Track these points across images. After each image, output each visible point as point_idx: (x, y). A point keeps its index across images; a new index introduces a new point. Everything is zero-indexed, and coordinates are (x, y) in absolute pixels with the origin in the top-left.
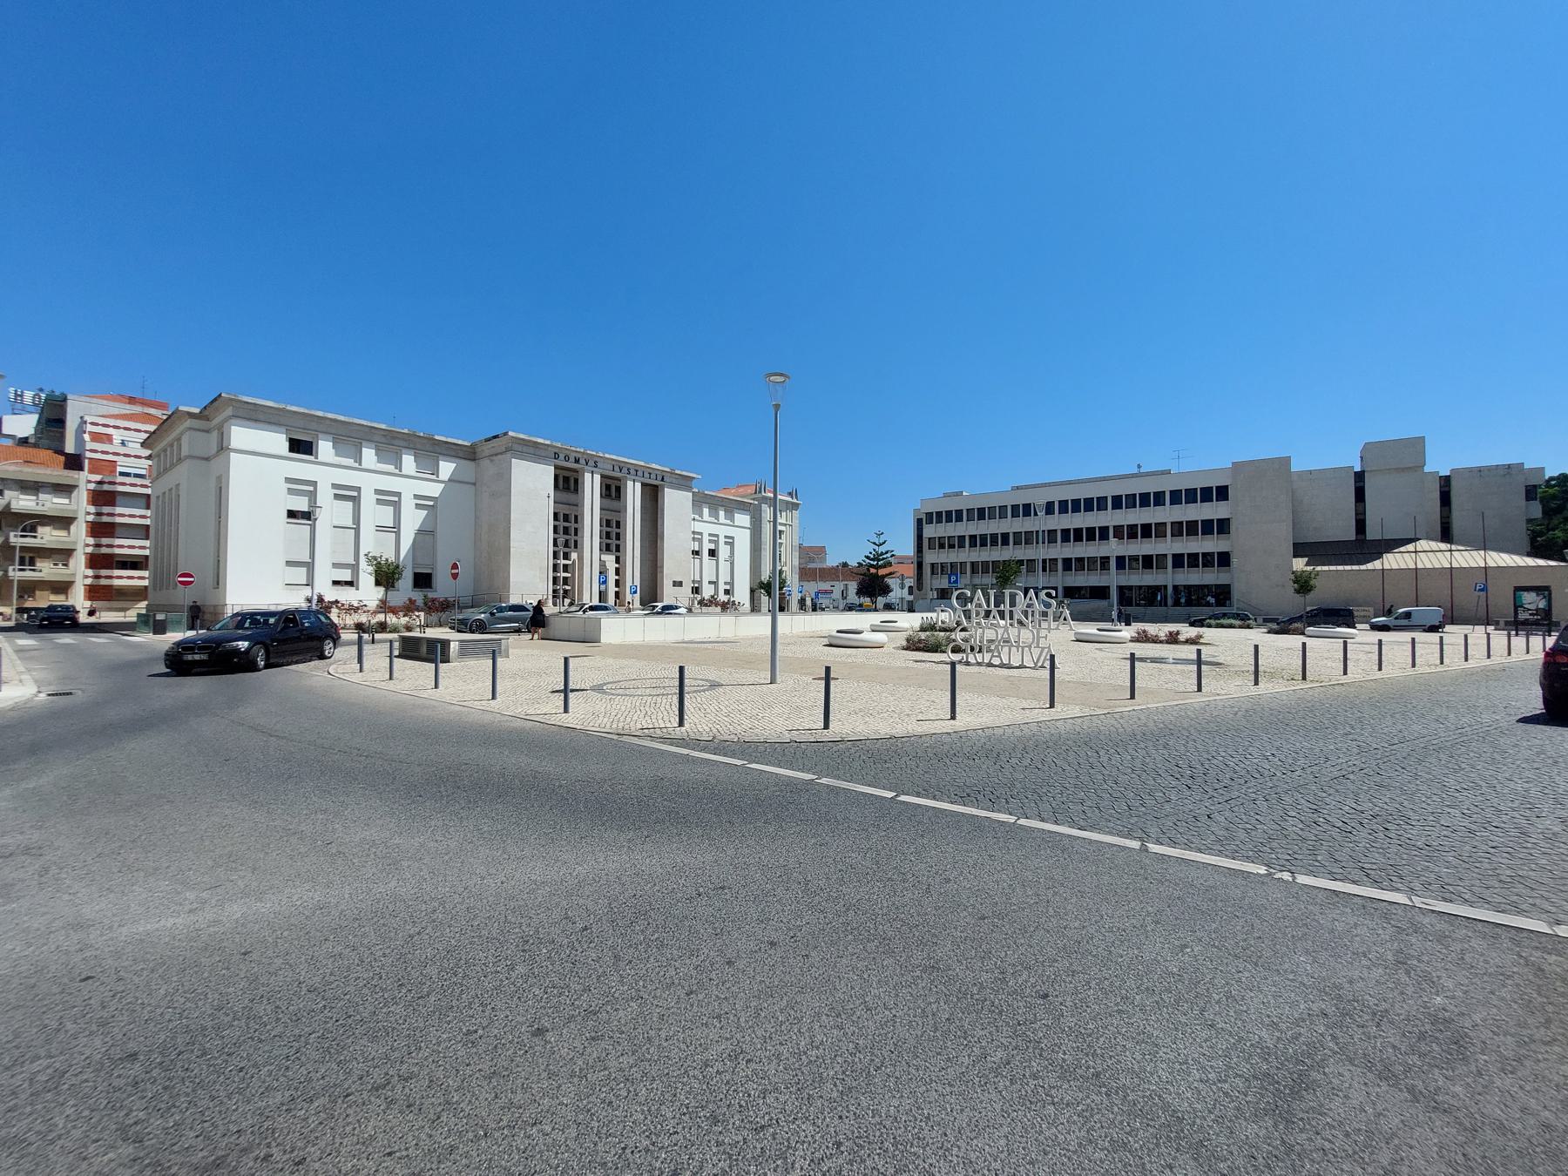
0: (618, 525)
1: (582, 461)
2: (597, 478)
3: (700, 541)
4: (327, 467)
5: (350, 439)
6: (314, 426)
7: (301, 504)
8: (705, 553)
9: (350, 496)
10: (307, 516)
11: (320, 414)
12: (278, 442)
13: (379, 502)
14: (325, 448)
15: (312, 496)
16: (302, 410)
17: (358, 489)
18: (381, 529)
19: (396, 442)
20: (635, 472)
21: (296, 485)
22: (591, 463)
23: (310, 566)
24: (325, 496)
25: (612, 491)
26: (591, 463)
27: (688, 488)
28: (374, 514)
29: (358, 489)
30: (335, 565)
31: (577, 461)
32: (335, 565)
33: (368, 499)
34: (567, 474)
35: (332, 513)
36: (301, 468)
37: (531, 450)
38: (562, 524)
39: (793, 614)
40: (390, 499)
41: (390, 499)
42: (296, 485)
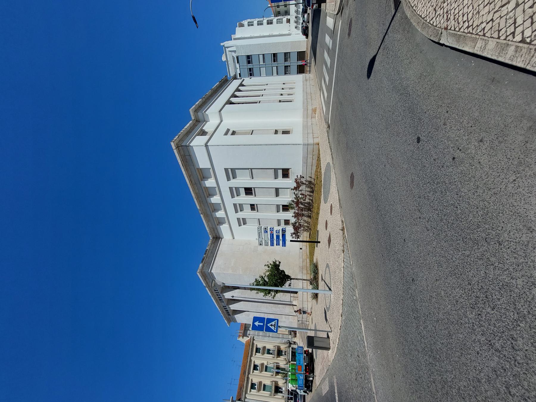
10: (277, 190)
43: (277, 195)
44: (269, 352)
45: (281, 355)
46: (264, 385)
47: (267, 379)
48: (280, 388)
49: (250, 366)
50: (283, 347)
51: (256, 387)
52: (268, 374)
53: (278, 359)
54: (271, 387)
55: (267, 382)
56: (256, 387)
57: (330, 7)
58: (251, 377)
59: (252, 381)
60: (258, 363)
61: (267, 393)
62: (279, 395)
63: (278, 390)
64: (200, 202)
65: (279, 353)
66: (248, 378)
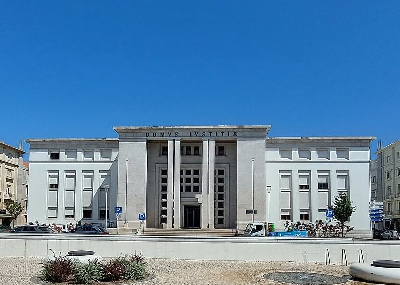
0: (197, 172)
3: (309, 178)
5: (71, 148)
7: (324, 181)
8: (315, 187)
9: (71, 175)
11: (57, 140)
12: (45, 156)
14: (63, 155)
15: (328, 177)
16: (50, 140)
17: (75, 172)
18: (85, 189)
19: (92, 146)
20: (175, 134)
22: (207, 134)
25: (191, 150)
26: (207, 134)
28: (82, 182)
29: (75, 172)
30: (282, 210)
31: (162, 135)
32: (282, 210)
33: (80, 175)
35: (65, 183)
36: (54, 166)
39: (173, 233)
40: (89, 174)
42: (54, 174)
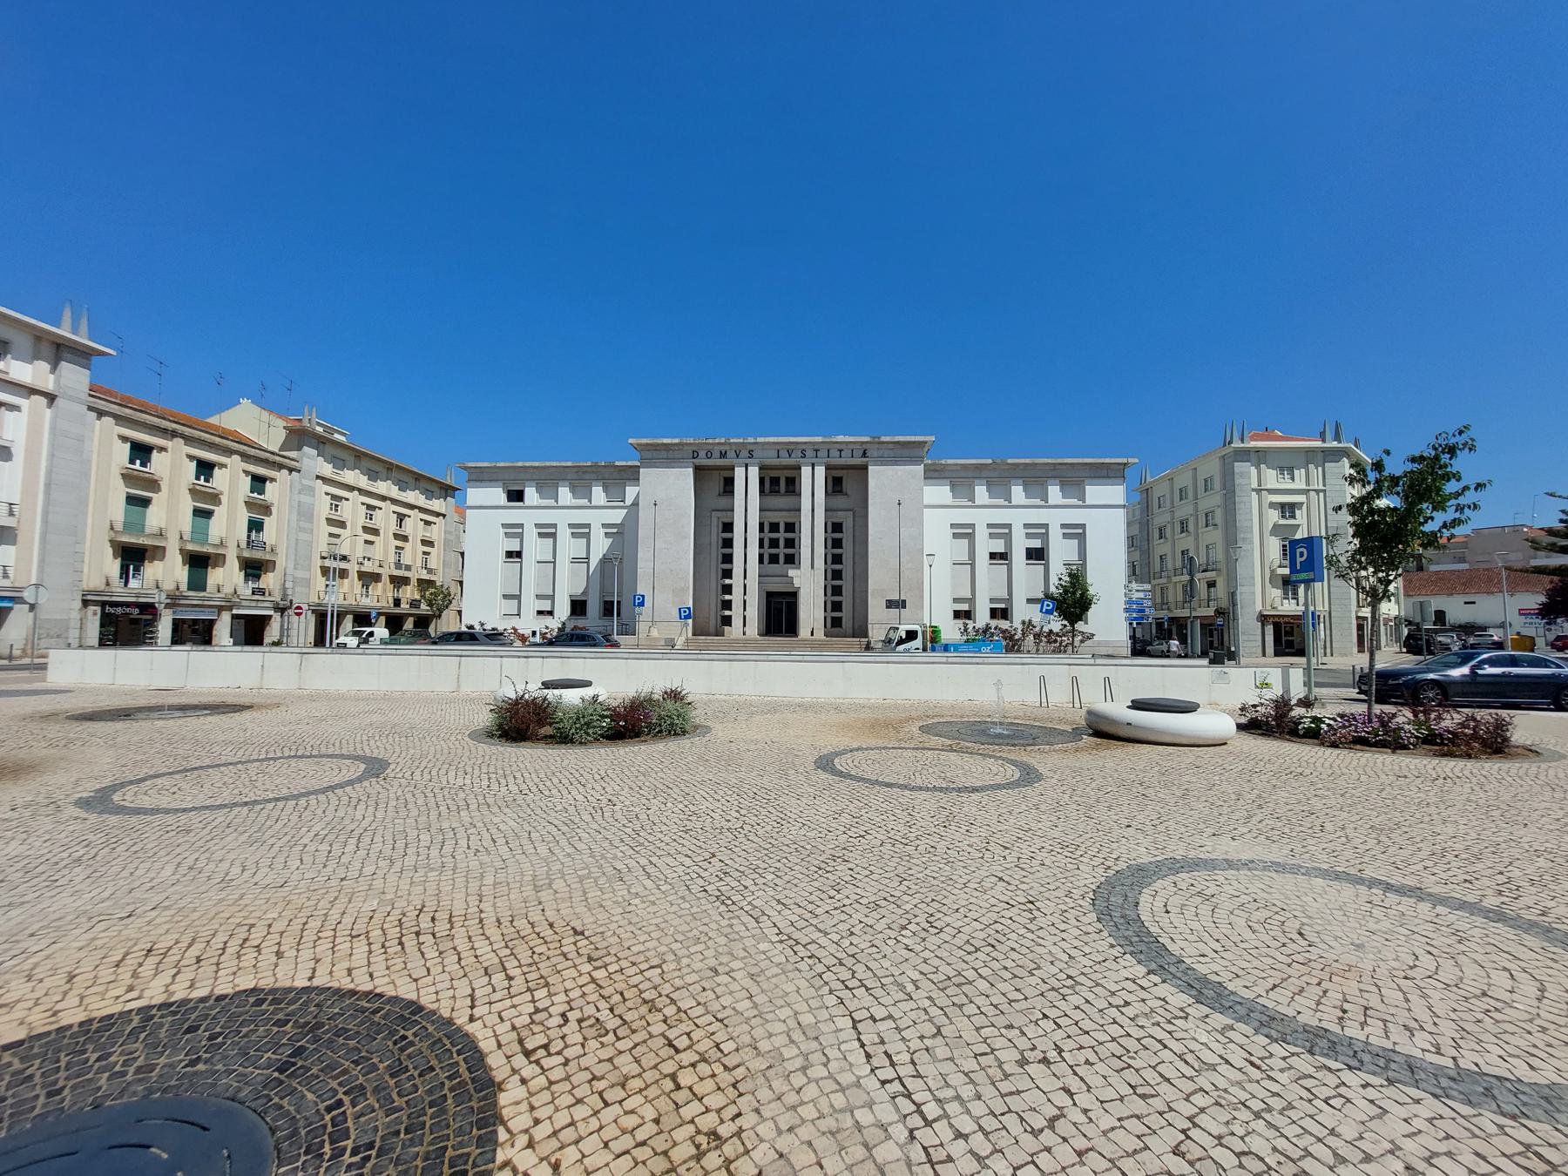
0: (791, 527)
1: (731, 454)
2: (820, 471)
3: (1008, 538)
4: (531, 514)
5: (548, 481)
6: (522, 476)
8: (1019, 556)
9: (548, 532)
10: (519, 554)
12: (498, 495)
13: (1065, 536)
14: (531, 494)
18: (575, 560)
21: (514, 530)
23: (518, 597)
24: (1055, 534)
25: (780, 484)
26: (744, 453)
27: (915, 460)
31: (723, 455)
32: (956, 600)
34: (774, 474)
35: (535, 548)
36: (515, 515)
37: (664, 454)
38: (768, 535)
39: (744, 644)
40: (581, 531)
41: (581, 531)
43: (891, 604)
44: (255, 526)
45: (247, 577)
46: (146, 502)
47: (169, 515)
48: (137, 570)
49: (211, 446)
50: (269, 580)
51: (137, 466)
52: (186, 521)
53: (180, 558)
54: (205, 542)
55: (155, 517)
56: (137, 466)
57: (3, 688)
58: (178, 447)
59: (162, 449)
60: (220, 479)
61: (117, 510)
62: (114, 567)
63: (133, 556)
64: (1499, 683)
65: (254, 568)
66: (174, 434)
